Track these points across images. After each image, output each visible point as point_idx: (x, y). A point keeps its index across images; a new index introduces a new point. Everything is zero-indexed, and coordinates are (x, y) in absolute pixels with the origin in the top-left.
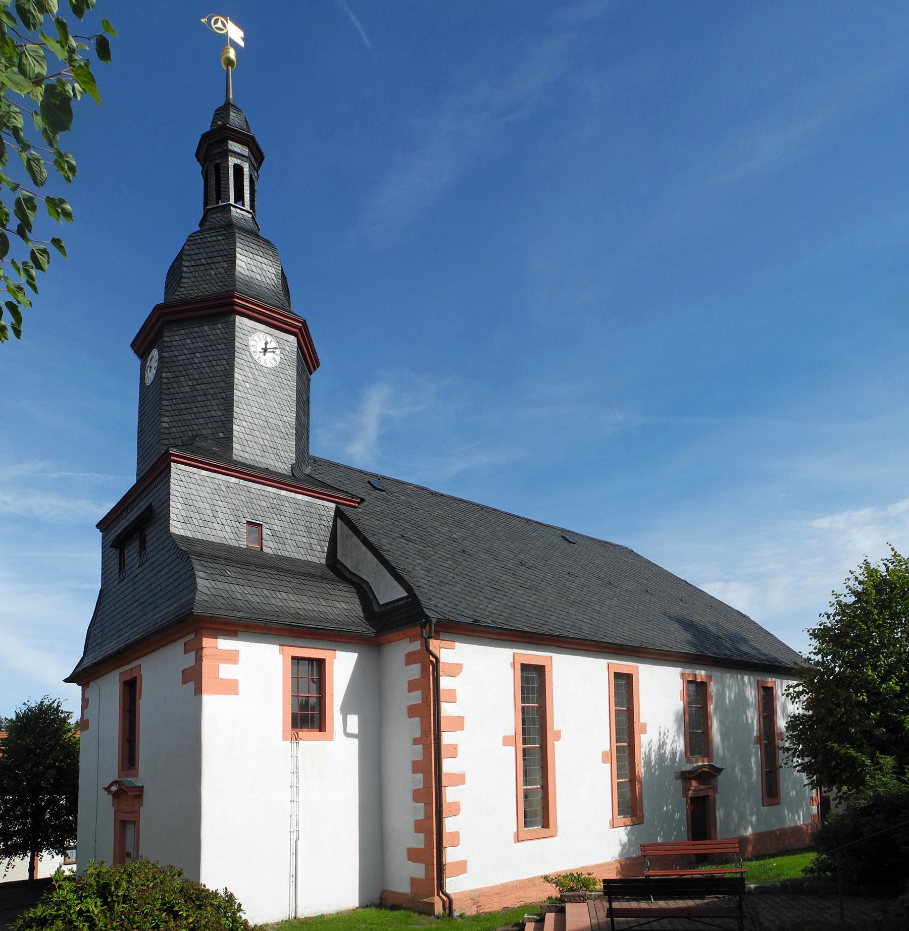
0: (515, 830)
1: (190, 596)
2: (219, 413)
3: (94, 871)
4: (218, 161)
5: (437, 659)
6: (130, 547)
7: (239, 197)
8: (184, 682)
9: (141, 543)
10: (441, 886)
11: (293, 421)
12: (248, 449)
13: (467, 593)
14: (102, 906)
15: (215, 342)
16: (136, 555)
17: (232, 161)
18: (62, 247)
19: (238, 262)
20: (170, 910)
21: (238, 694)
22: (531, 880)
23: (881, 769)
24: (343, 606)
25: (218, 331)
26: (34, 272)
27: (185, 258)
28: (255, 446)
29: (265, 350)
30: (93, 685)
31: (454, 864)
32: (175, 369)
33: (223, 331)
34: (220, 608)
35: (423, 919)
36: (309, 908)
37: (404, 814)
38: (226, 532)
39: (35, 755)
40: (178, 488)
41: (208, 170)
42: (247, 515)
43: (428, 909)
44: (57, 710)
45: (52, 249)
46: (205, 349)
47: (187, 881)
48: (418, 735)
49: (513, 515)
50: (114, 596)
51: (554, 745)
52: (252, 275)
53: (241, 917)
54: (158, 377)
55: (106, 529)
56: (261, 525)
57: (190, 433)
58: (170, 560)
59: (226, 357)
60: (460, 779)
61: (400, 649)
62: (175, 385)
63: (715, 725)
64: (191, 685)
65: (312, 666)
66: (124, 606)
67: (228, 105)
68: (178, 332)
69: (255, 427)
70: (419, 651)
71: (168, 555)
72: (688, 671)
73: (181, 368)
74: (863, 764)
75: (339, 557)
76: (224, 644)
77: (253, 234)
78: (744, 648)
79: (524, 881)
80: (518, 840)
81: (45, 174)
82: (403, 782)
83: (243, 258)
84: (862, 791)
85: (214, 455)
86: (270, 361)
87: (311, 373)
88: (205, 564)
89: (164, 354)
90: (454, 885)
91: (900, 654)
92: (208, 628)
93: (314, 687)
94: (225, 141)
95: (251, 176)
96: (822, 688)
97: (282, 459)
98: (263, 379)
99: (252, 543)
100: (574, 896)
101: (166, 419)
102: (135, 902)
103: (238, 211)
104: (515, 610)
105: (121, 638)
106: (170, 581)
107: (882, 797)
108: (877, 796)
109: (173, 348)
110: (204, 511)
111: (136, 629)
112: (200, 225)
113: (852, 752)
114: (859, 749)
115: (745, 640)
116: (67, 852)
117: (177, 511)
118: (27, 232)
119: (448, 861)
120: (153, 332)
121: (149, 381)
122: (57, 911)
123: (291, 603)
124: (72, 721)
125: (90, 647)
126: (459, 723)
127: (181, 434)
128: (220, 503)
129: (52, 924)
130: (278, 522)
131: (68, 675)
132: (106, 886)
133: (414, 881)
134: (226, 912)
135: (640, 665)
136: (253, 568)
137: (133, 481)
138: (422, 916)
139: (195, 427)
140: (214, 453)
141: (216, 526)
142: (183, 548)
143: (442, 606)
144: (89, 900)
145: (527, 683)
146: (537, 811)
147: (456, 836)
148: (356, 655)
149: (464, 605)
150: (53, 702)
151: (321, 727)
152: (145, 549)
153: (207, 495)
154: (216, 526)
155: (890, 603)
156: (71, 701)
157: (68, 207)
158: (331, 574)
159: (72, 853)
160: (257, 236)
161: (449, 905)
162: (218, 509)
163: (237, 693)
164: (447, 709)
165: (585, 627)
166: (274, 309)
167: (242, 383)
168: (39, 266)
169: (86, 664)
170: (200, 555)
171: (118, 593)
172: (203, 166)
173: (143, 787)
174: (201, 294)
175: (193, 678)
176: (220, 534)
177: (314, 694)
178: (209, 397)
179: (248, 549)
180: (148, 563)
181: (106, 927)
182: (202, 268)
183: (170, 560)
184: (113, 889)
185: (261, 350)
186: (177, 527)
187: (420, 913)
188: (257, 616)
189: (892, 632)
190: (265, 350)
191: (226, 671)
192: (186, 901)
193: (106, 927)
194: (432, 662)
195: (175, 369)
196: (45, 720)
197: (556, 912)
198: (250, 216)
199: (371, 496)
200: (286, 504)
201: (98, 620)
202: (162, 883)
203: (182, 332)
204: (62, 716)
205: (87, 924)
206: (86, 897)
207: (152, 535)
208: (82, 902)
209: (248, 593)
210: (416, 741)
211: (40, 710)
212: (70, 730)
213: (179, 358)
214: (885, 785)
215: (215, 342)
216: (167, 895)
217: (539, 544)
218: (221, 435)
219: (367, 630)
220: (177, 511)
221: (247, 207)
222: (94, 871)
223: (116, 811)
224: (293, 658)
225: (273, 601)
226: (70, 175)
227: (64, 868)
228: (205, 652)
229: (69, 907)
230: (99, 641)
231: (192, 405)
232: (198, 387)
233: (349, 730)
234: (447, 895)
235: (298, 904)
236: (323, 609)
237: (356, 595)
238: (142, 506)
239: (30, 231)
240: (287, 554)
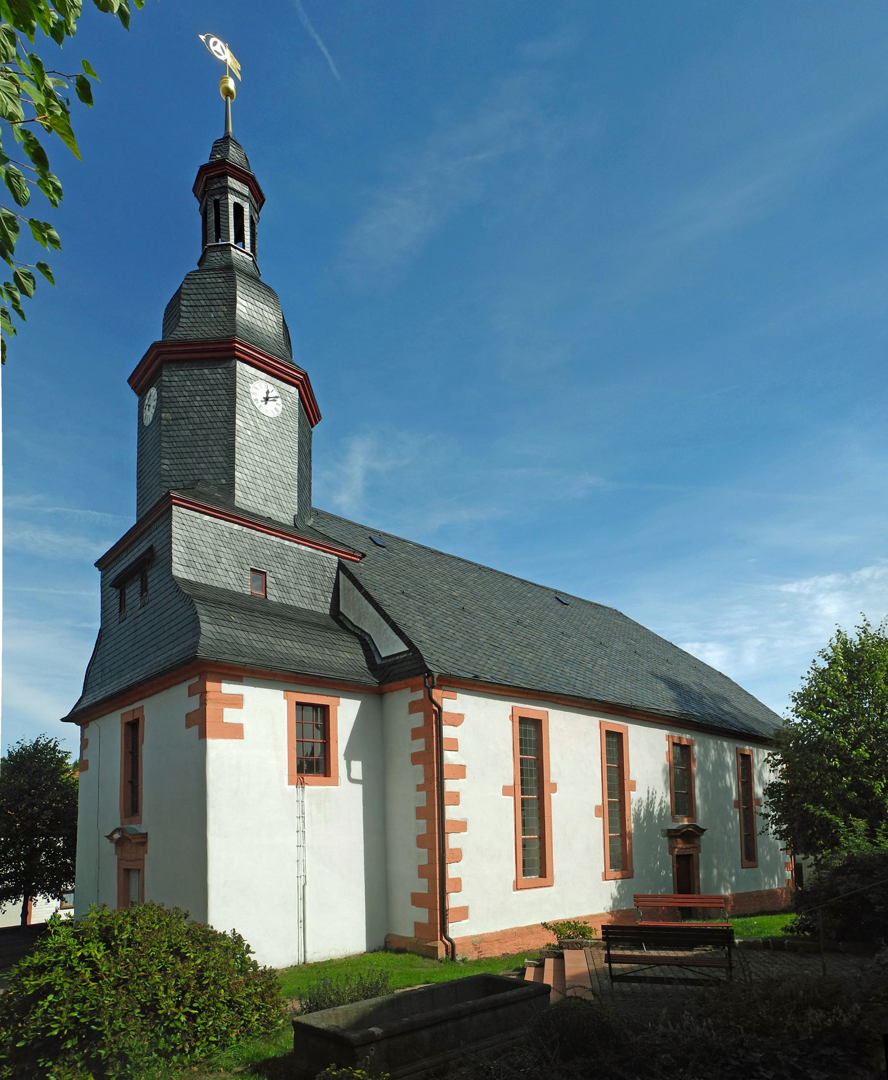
0: (514, 878)
1: (195, 639)
2: (221, 459)
3: (95, 915)
4: (217, 197)
5: (440, 709)
6: (131, 588)
7: (239, 237)
8: (188, 726)
9: (142, 584)
10: (444, 931)
11: (295, 472)
12: (250, 497)
13: (467, 649)
14: (105, 950)
15: (216, 387)
16: (137, 596)
17: (232, 199)
18: (49, 273)
19: (238, 305)
20: (177, 953)
22: (529, 928)
23: (853, 831)
24: (347, 657)
25: (218, 376)
26: (18, 295)
27: (182, 296)
28: (257, 494)
29: (267, 399)
30: (92, 725)
31: (456, 910)
32: (175, 410)
33: (224, 376)
34: (225, 653)
35: (427, 962)
36: (318, 952)
37: (408, 859)
38: (229, 577)
39: (30, 795)
40: (180, 532)
41: (207, 204)
43: (432, 954)
44: (54, 749)
45: (38, 274)
46: (205, 393)
47: (193, 923)
48: (421, 781)
49: (510, 576)
50: (115, 636)
52: (253, 320)
53: (249, 959)
54: (157, 416)
55: (105, 568)
56: (265, 573)
57: (191, 477)
58: (172, 603)
59: (227, 403)
60: (462, 826)
61: (401, 700)
62: (175, 428)
63: (697, 783)
64: (195, 729)
65: (317, 711)
66: (126, 647)
67: (226, 139)
68: (177, 373)
69: (257, 475)
70: (422, 700)
71: (170, 597)
72: (676, 735)
73: (181, 410)
74: (837, 826)
75: (341, 610)
76: (228, 688)
77: (254, 278)
78: (725, 707)
79: (522, 928)
80: (517, 888)
81: (27, 193)
82: (407, 828)
83: (244, 302)
84: (836, 852)
85: (216, 501)
86: (272, 410)
87: (313, 426)
88: (209, 608)
89: (164, 394)
90: (457, 930)
91: (869, 723)
92: (212, 672)
93: (318, 733)
94: (224, 176)
95: (251, 217)
96: (798, 752)
97: (284, 510)
99: (257, 589)
100: (571, 943)
101: (166, 461)
102: (140, 944)
103: (239, 252)
104: (513, 667)
105: (123, 679)
106: (173, 623)
107: (856, 858)
108: (851, 857)
109: (173, 389)
110: (207, 556)
111: (138, 670)
112: (199, 264)
113: (826, 813)
114: (833, 811)
115: (726, 700)
116: (64, 896)
117: (179, 554)
118: (9, 254)
120: (151, 370)
121: (147, 422)
122: (56, 957)
123: (296, 651)
124: (71, 761)
125: (89, 686)
126: (460, 772)
127: (182, 478)
128: (223, 549)
129: (51, 971)
130: (282, 571)
131: (65, 714)
132: (109, 929)
133: (418, 926)
134: (235, 954)
135: (629, 725)
136: (257, 614)
137: (133, 521)
138: (426, 960)
139: (196, 472)
140: (217, 499)
141: (220, 571)
142: (186, 592)
143: (444, 661)
144: (91, 944)
145: (525, 736)
146: (534, 862)
147: (458, 882)
148: (359, 702)
149: (465, 661)
150: (50, 742)
151: (327, 773)
152: (147, 591)
153: (210, 540)
154: (220, 571)
155: (858, 675)
156: (69, 740)
157: (54, 233)
158: (335, 625)
159: (69, 898)
160: (258, 281)
161: (451, 949)
162: (221, 554)
163: (242, 737)
165: (579, 685)
166: (275, 358)
167: (244, 430)
168: (24, 291)
169: (85, 704)
170: (204, 599)
171: (120, 632)
172: (201, 203)
174: (200, 336)
175: (198, 723)
176: (224, 579)
177: (319, 739)
178: (211, 442)
179: (252, 596)
180: (150, 604)
181: (109, 971)
182: (201, 309)
183: (172, 603)
184: (116, 933)
185: (263, 400)
186: (179, 570)
187: (424, 957)
188: (262, 662)
189: (860, 702)
190: (267, 399)
191: (230, 715)
192: (193, 943)
193: (109, 971)
194: (435, 711)
195: (175, 410)
196: (40, 760)
197: (555, 958)
198: (251, 259)
199: (372, 552)
200: (290, 553)
201: (97, 659)
202: (168, 925)
203: (182, 373)
204: (60, 756)
205: (89, 969)
206: (87, 942)
207: (153, 576)
208: (83, 947)
209: (254, 640)
210: (419, 788)
211: (35, 749)
212: (67, 770)
213: (179, 399)
214: (858, 846)
215: (216, 387)
216: (173, 937)
217: (534, 604)
218: (223, 481)
219: (371, 680)
220: (179, 554)
221: (248, 249)
222: (95, 915)
223: (119, 860)
224: (298, 704)
225: (278, 648)
226: (56, 198)
227: (62, 913)
228: (209, 696)
229: (70, 953)
230: (99, 681)
231: (193, 449)
232: (199, 432)
233: (353, 776)
234: (449, 940)
235: (308, 949)
236: (327, 658)
237: (359, 646)
238: (143, 547)
239: (12, 253)
240: (291, 603)
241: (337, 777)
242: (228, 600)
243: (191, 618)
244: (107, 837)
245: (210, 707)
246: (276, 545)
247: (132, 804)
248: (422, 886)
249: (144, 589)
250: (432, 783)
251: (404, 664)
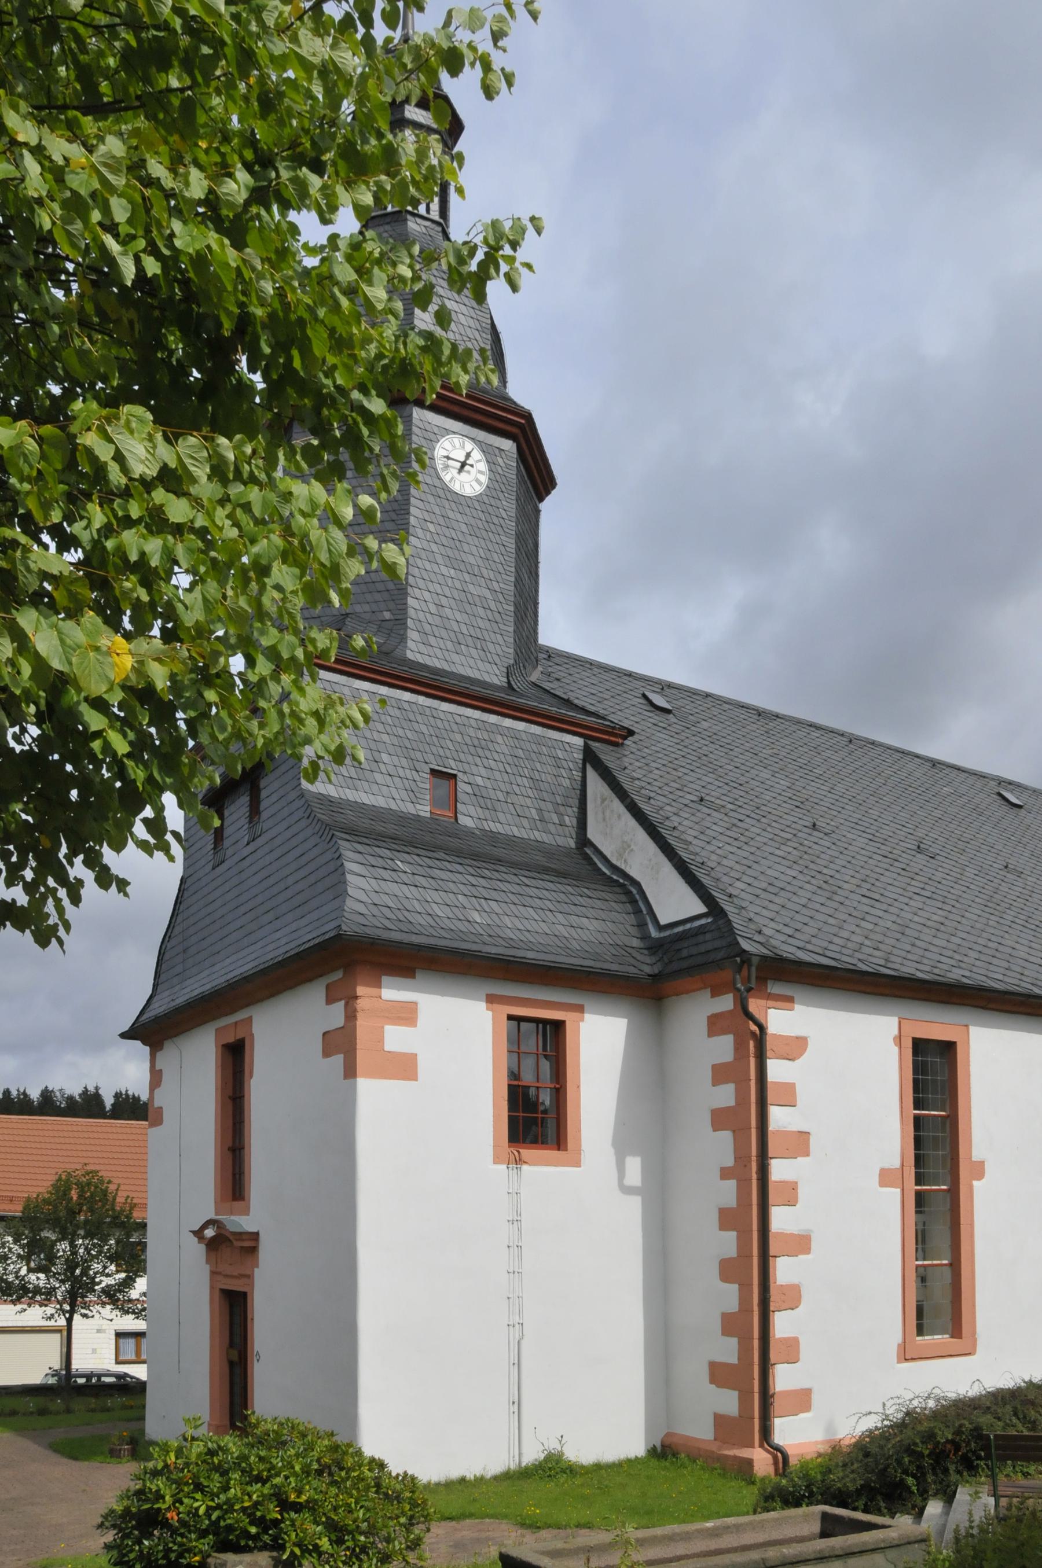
5: (762, 1028)
6: (232, 808)
8: (327, 1053)
9: (251, 800)
10: (766, 1432)
16: (244, 821)
21: (416, 1080)
42: (430, 758)
48: (730, 1162)
51: (971, 1187)
56: (455, 776)
60: (801, 1244)
61: (696, 1011)
64: (338, 1059)
76: (393, 992)
80: (906, 1355)
87: (541, 500)
93: (546, 1066)
98: (459, 517)
119: (777, 1389)
125: (163, 977)
126: (800, 1144)
133: (720, 1421)
164: (779, 1117)
169: (160, 1008)
170: (354, 833)
173: (257, 1234)
175: (341, 1045)
191: (396, 1038)
194: (753, 1034)
200: (499, 739)
201: (177, 930)
210: (725, 1174)
224: (510, 1018)
228: (361, 1004)
234: (778, 1449)
241: (579, 1151)
242: (391, 829)
243: (332, 867)
244: (195, 1233)
245: (362, 1023)
246: (473, 723)
247: (234, 1183)
248: (727, 1350)
249: (255, 810)
250: (747, 1165)
251: (701, 938)
